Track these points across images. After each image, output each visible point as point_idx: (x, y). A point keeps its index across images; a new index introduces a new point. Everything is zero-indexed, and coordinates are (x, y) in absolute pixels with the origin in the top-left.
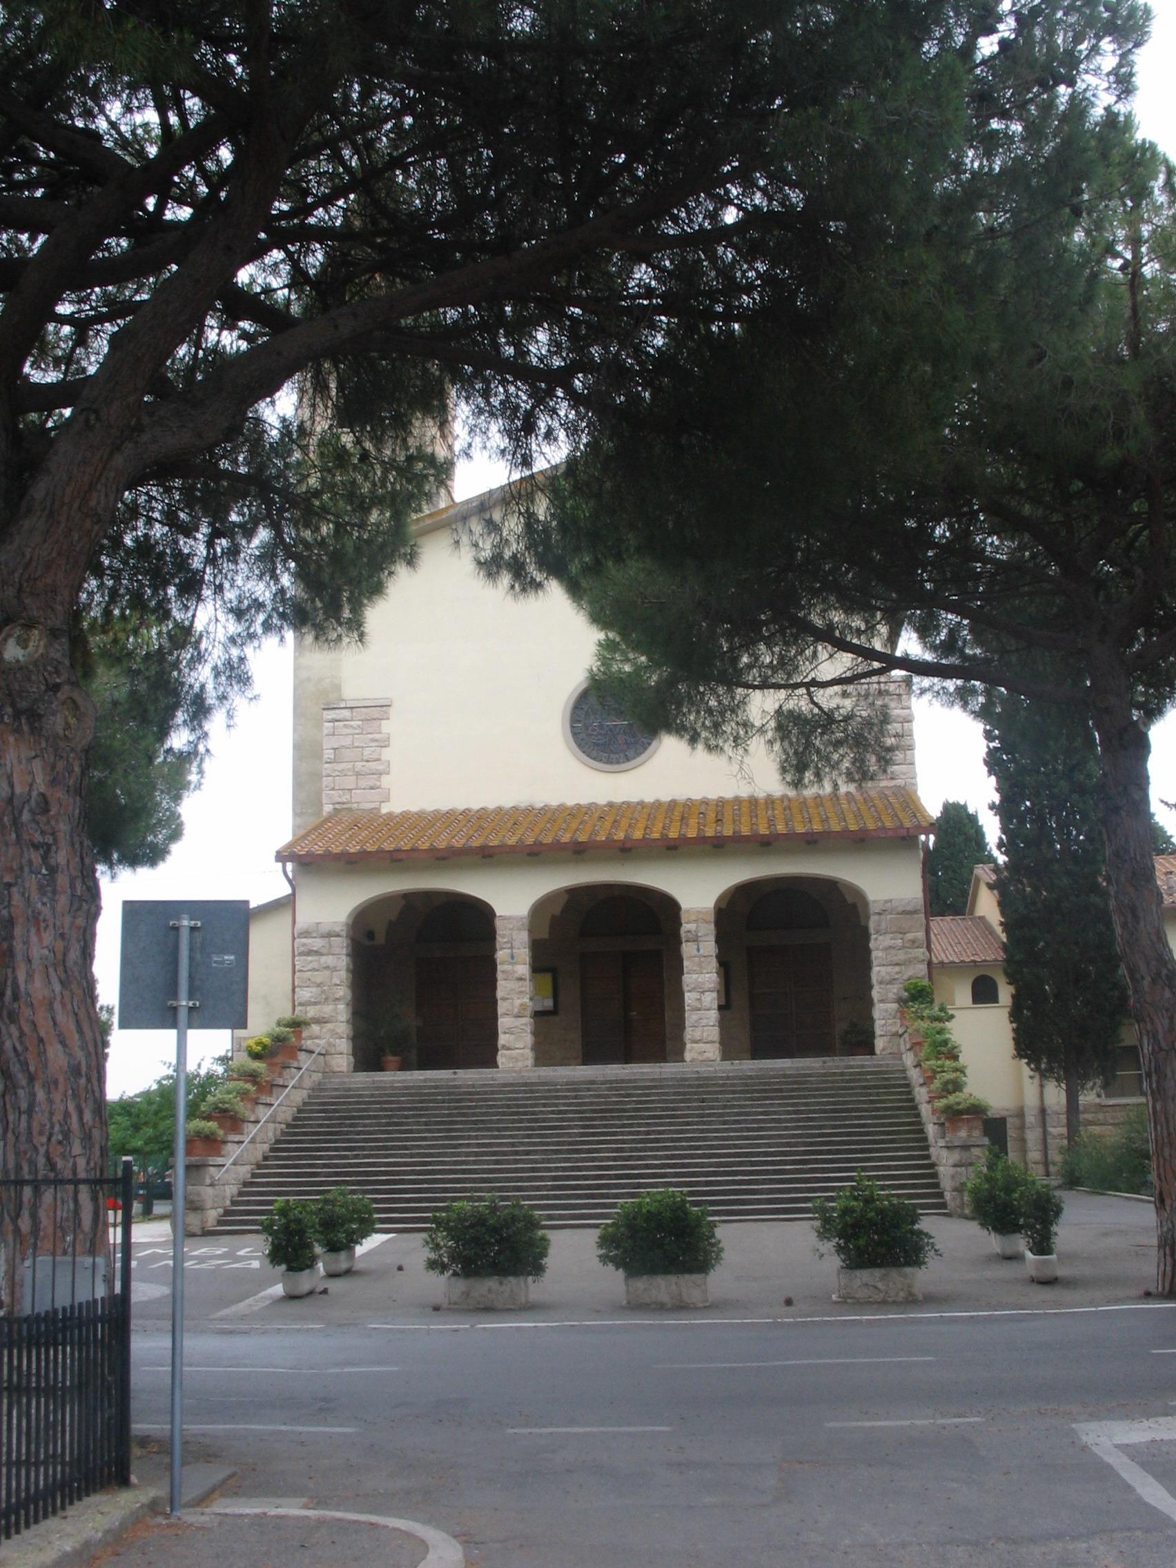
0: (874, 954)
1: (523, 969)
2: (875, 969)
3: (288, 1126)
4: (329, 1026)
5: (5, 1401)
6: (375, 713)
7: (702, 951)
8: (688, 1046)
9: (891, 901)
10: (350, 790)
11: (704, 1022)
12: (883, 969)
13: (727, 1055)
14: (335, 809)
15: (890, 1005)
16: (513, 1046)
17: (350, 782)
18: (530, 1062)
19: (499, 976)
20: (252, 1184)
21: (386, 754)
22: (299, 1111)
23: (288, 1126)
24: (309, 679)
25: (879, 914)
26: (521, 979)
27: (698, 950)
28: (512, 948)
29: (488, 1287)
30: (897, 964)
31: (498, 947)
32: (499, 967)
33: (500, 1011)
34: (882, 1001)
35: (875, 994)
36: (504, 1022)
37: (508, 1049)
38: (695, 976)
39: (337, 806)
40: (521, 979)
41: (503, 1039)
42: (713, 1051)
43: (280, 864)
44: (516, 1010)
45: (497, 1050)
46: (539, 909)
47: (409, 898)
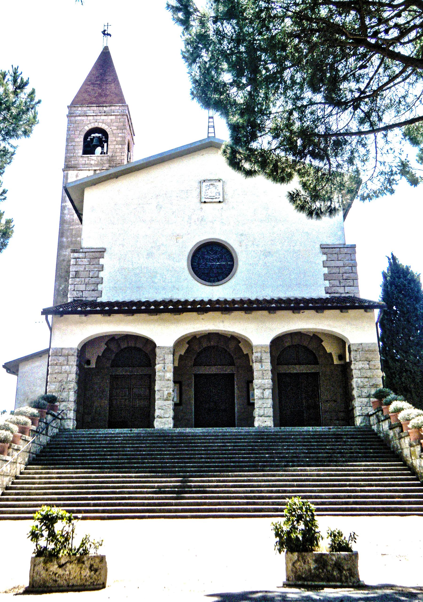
0: (354, 372)
1: (170, 375)
2: (355, 380)
3: (37, 455)
4: (64, 403)
5: (189, 484)
6: (97, 254)
7: (263, 367)
8: (257, 418)
9: (361, 344)
10: (82, 291)
11: (265, 405)
12: (359, 380)
13: (275, 426)
14: (74, 300)
15: (363, 399)
16: (163, 416)
17: (82, 287)
18: (172, 425)
19: (157, 378)
20: (11, 488)
21: (101, 274)
22: (44, 448)
23: (37, 455)
24: (64, 260)
25: (356, 351)
26: (168, 380)
27: (262, 367)
28: (164, 363)
29: (284, 595)
30: (366, 377)
31: (157, 362)
32: (157, 373)
33: (157, 397)
34: (359, 397)
35: (355, 393)
36: (158, 403)
37: (161, 418)
38: (260, 381)
39: (75, 299)
40: (168, 380)
41: (157, 413)
42: (269, 423)
43: (44, 316)
44: (165, 397)
45: (154, 418)
46: (179, 343)
47: (112, 339)
